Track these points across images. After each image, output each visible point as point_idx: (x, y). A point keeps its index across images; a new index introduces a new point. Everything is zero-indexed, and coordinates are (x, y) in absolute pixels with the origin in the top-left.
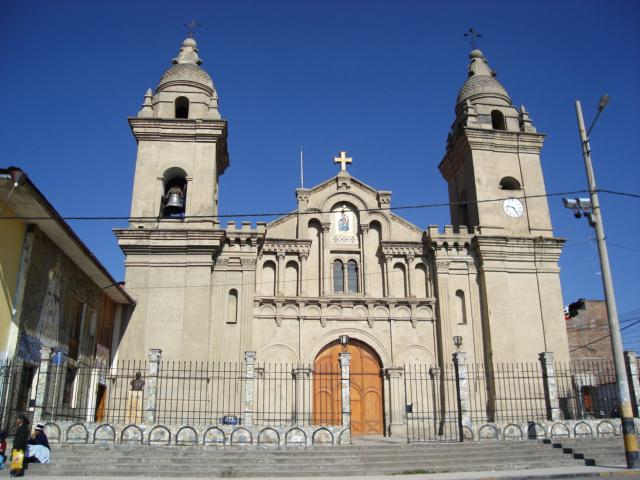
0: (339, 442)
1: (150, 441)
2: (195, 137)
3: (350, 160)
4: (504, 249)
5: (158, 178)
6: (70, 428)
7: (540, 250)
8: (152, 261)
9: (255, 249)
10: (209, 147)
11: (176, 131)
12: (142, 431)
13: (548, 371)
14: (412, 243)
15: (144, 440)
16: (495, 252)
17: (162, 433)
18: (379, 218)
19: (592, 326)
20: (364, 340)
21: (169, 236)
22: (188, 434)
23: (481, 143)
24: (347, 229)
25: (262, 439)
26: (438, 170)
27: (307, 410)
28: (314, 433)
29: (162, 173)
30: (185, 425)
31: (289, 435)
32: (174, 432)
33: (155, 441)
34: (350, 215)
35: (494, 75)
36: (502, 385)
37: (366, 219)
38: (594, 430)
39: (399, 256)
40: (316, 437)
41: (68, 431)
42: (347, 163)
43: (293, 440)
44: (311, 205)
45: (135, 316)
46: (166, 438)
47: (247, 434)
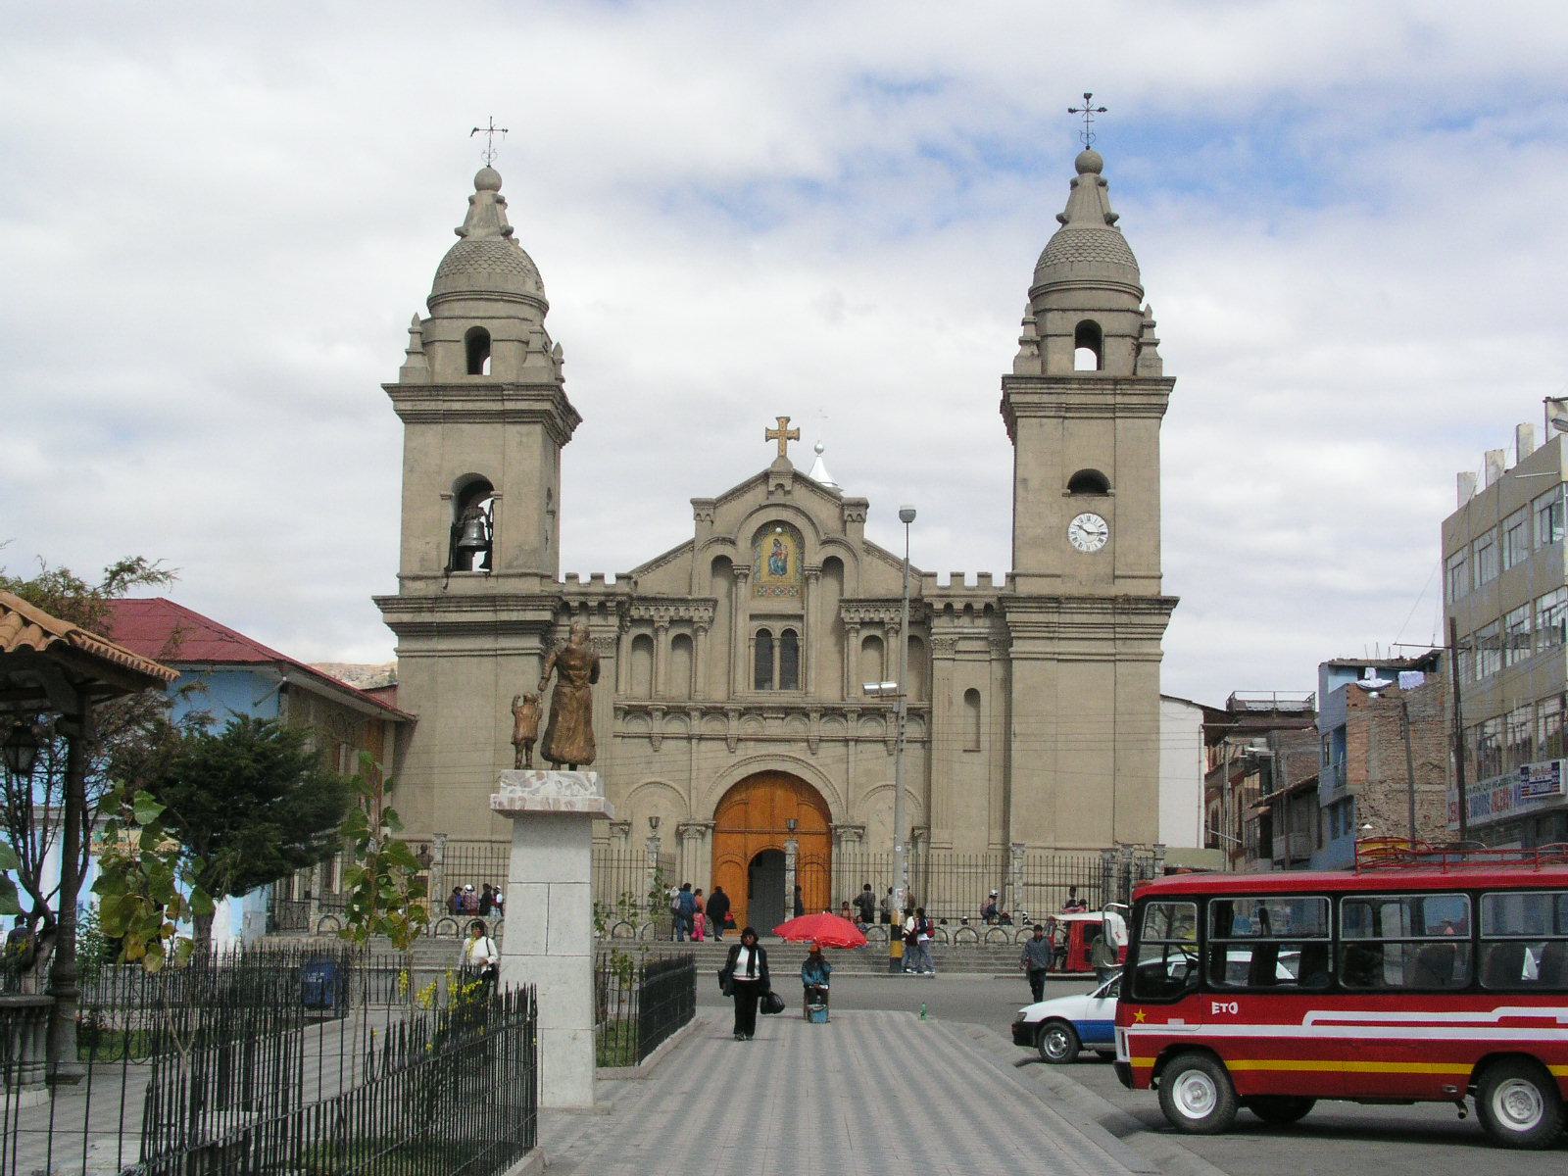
1: (436, 934)
4: (1055, 618)
5: (444, 497)
7: (1124, 619)
8: (440, 647)
9: (614, 621)
15: (430, 933)
17: (450, 926)
18: (840, 553)
19: (17, 1068)
20: (799, 775)
23: (1038, 406)
24: (784, 569)
29: (450, 485)
34: (787, 542)
37: (815, 557)
38: (951, 938)
45: (418, 739)
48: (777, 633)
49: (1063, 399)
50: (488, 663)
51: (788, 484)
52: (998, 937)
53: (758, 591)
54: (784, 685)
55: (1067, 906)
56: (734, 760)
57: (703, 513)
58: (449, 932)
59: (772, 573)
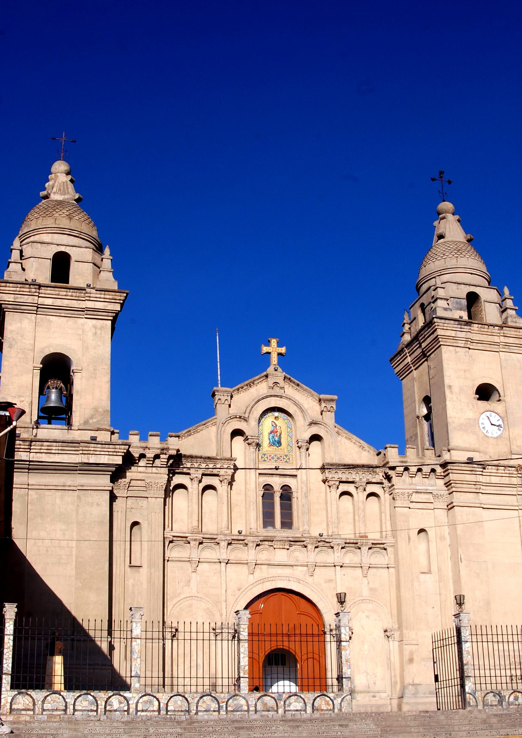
0: (340, 710)
1: (137, 711)
2: (82, 310)
3: (283, 350)
4: (481, 479)
6: (46, 697)
10: (102, 328)
11: (58, 302)
13: (241, 649)
14: (363, 466)
15: (131, 710)
16: (468, 482)
17: (151, 702)
21: (55, 447)
23: (454, 338)
24: (279, 443)
25: (259, 708)
28: (315, 700)
30: (175, 692)
31: (287, 702)
32: (163, 702)
35: (469, 241)
40: (316, 704)
41: (43, 702)
42: (279, 354)
43: (292, 708)
44: (233, 411)
46: (156, 708)
48: (277, 488)
49: (469, 335)
50: (70, 497)
55: (182, 734)
56: (252, 579)
58: (151, 709)
59: (272, 444)
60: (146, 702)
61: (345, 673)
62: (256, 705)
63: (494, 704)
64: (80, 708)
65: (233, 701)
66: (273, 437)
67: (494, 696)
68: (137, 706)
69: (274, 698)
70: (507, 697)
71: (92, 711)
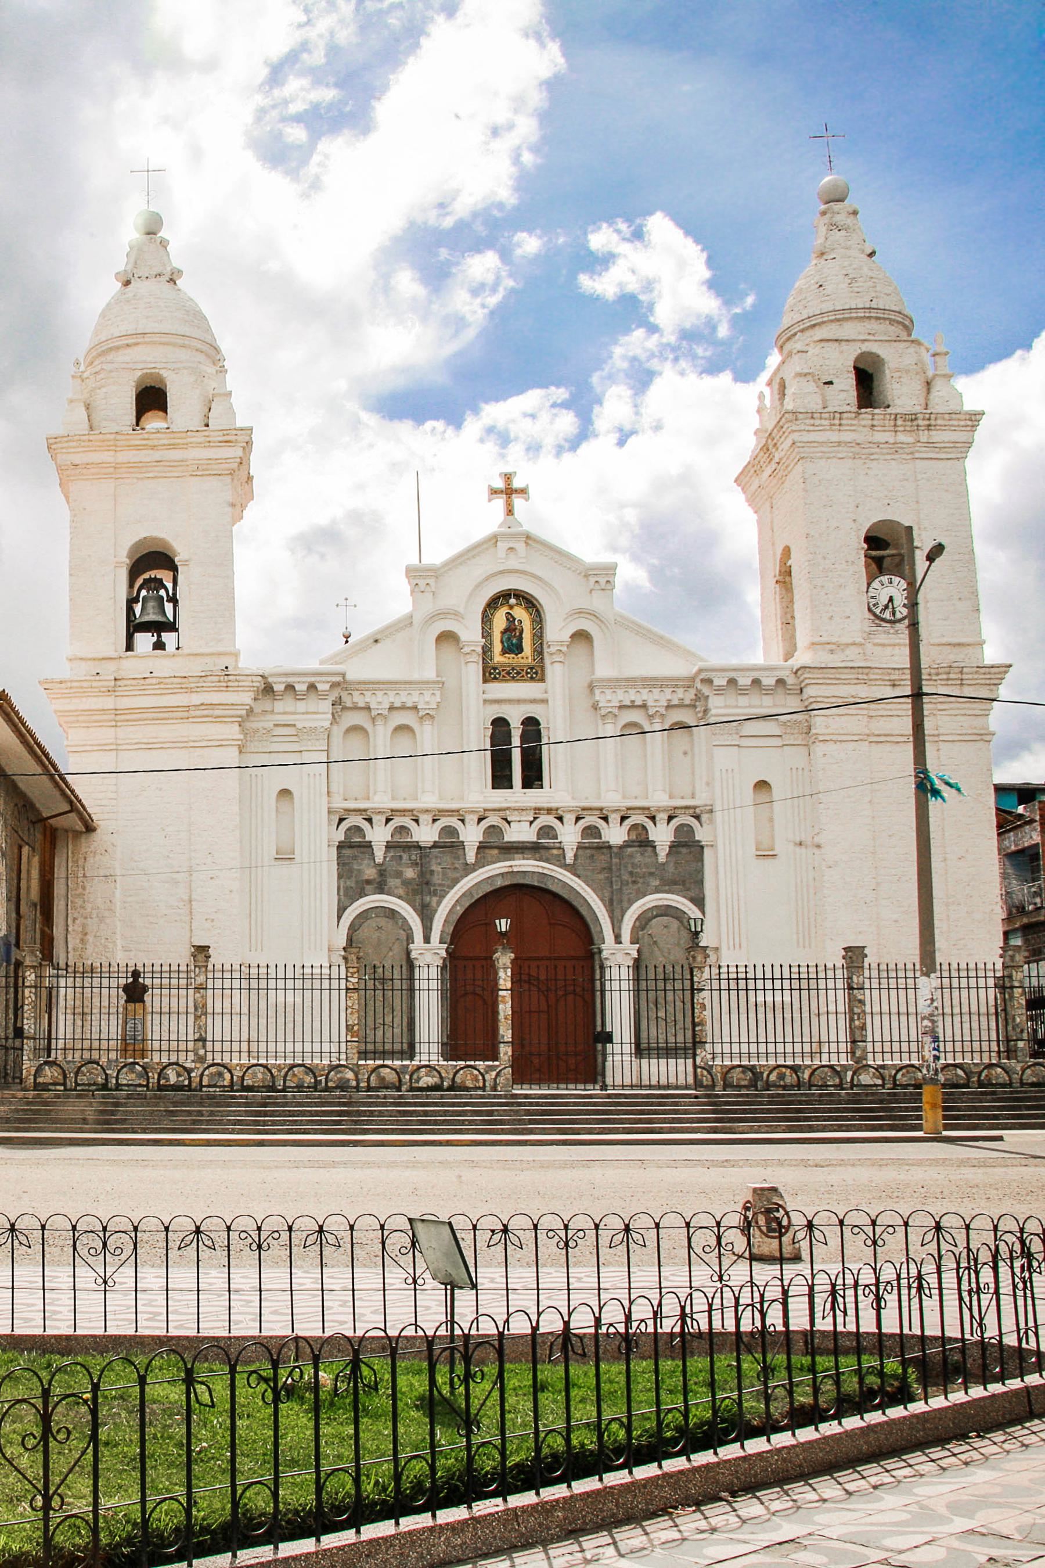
12: (189, 1071)
15: (194, 1085)
17: (220, 1075)
22: (260, 1076)
24: (519, 649)
26: (738, 384)
27: (113, 1036)
31: (415, 1076)
33: (209, 1086)
34: (520, 614)
36: (618, 1064)
39: (633, 706)
41: (77, 1074)
47: (350, 1075)
51: (520, 546)
52: (997, 1076)
53: (491, 674)
54: (527, 784)
57: (422, 583)
58: (220, 1083)
59: (504, 652)
60: (211, 1075)
61: (503, 1036)
62: (369, 1078)
63: (743, 1083)
64: (125, 1082)
65: (336, 1074)
66: (509, 639)
67: (743, 1072)
68: (201, 1080)
69: (395, 1070)
70: (765, 1075)
71: (140, 1085)
